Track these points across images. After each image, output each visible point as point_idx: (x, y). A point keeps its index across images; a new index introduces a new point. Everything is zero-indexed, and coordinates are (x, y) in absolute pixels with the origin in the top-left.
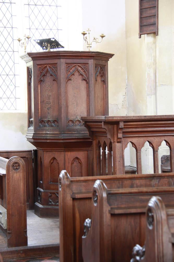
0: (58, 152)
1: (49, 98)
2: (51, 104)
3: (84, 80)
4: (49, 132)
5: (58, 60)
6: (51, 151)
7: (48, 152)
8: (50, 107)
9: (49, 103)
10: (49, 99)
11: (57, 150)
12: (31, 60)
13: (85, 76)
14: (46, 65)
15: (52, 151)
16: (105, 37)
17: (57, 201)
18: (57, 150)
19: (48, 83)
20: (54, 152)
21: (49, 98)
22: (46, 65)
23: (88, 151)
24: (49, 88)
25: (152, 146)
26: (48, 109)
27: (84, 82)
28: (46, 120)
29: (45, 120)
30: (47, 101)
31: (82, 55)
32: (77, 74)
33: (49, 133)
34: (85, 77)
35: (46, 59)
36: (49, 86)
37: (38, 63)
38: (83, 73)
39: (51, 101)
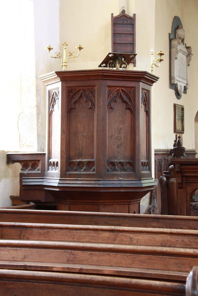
0: (121, 206)
1: (119, 131)
2: (123, 140)
3: (129, 109)
4: (122, 178)
5: (137, 83)
6: (111, 204)
7: (107, 206)
8: (121, 144)
9: (120, 138)
10: (120, 134)
11: (121, 202)
12: (60, 80)
13: (129, 103)
14: (119, 88)
15: (113, 205)
16: (164, 55)
17: (187, 269)
18: (121, 202)
19: (119, 112)
20: (115, 206)
21: (119, 131)
22: (119, 88)
23: (99, 205)
24: (121, 119)
25: (194, 192)
26: (118, 147)
27: (128, 112)
28: (117, 162)
29: (115, 162)
30: (117, 135)
31: (129, 75)
32: (119, 100)
33: (121, 179)
34: (130, 105)
35: (69, 81)
36: (120, 115)
37: (109, 85)
38: (128, 101)
39: (122, 136)
